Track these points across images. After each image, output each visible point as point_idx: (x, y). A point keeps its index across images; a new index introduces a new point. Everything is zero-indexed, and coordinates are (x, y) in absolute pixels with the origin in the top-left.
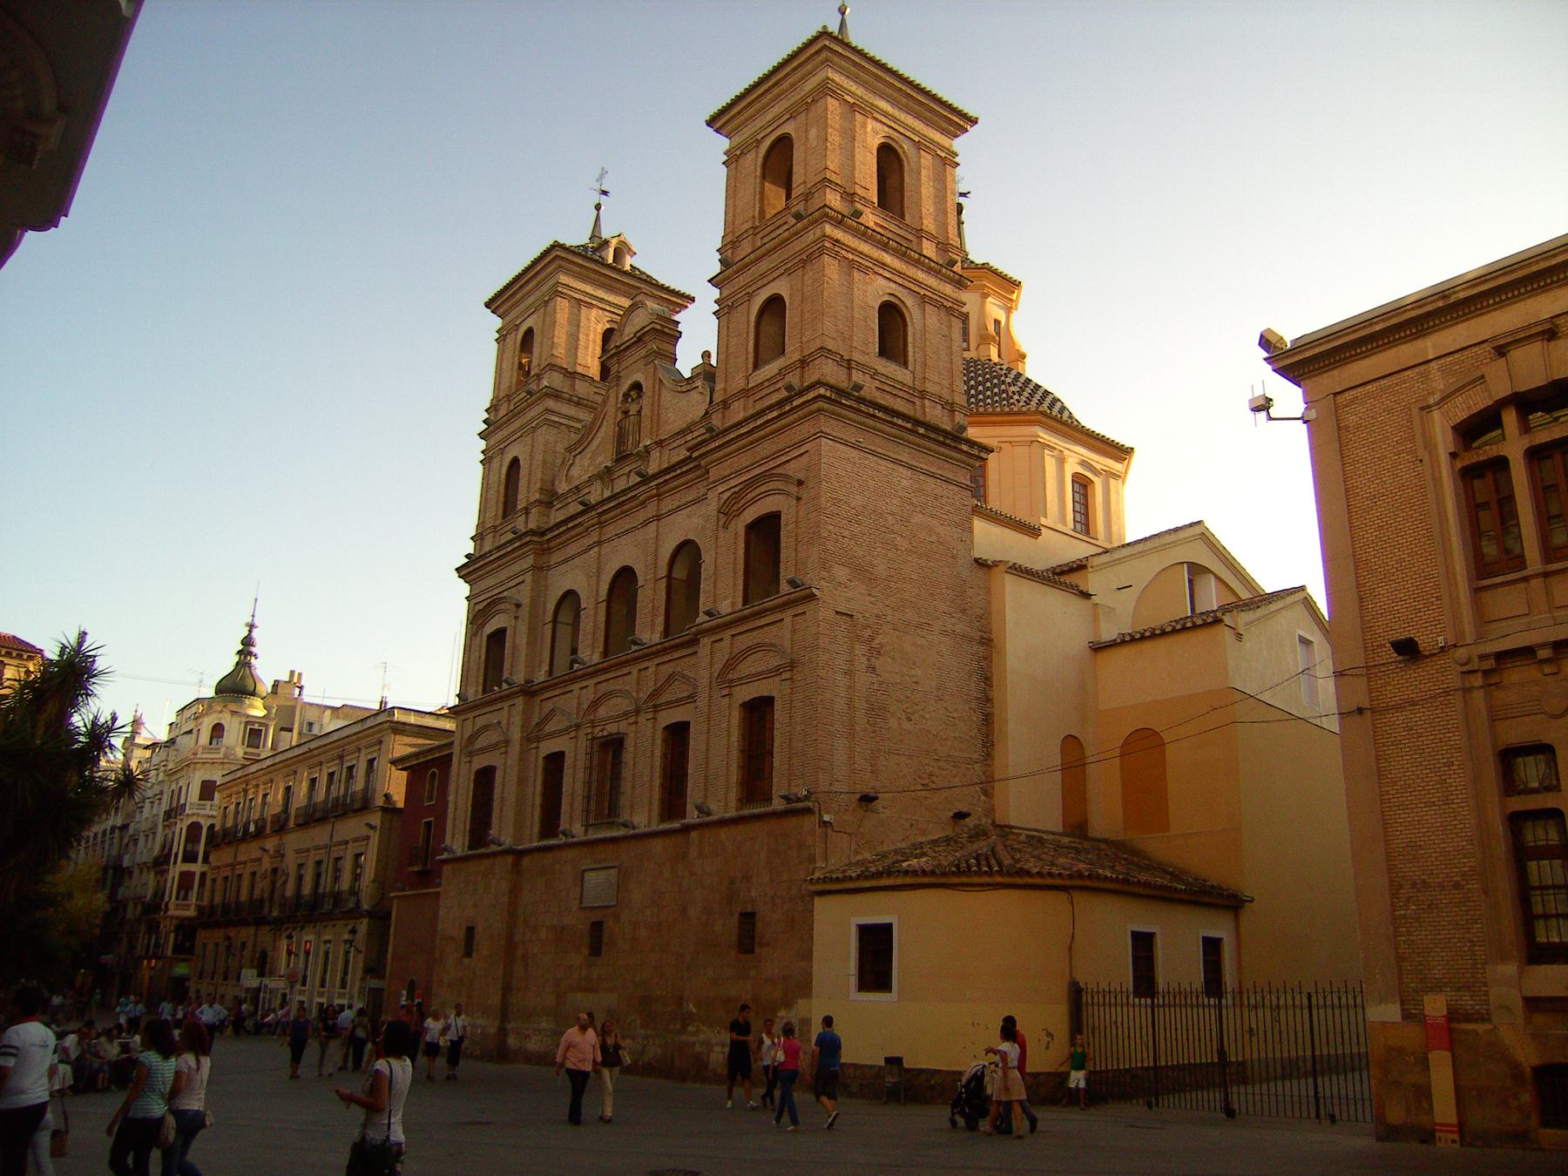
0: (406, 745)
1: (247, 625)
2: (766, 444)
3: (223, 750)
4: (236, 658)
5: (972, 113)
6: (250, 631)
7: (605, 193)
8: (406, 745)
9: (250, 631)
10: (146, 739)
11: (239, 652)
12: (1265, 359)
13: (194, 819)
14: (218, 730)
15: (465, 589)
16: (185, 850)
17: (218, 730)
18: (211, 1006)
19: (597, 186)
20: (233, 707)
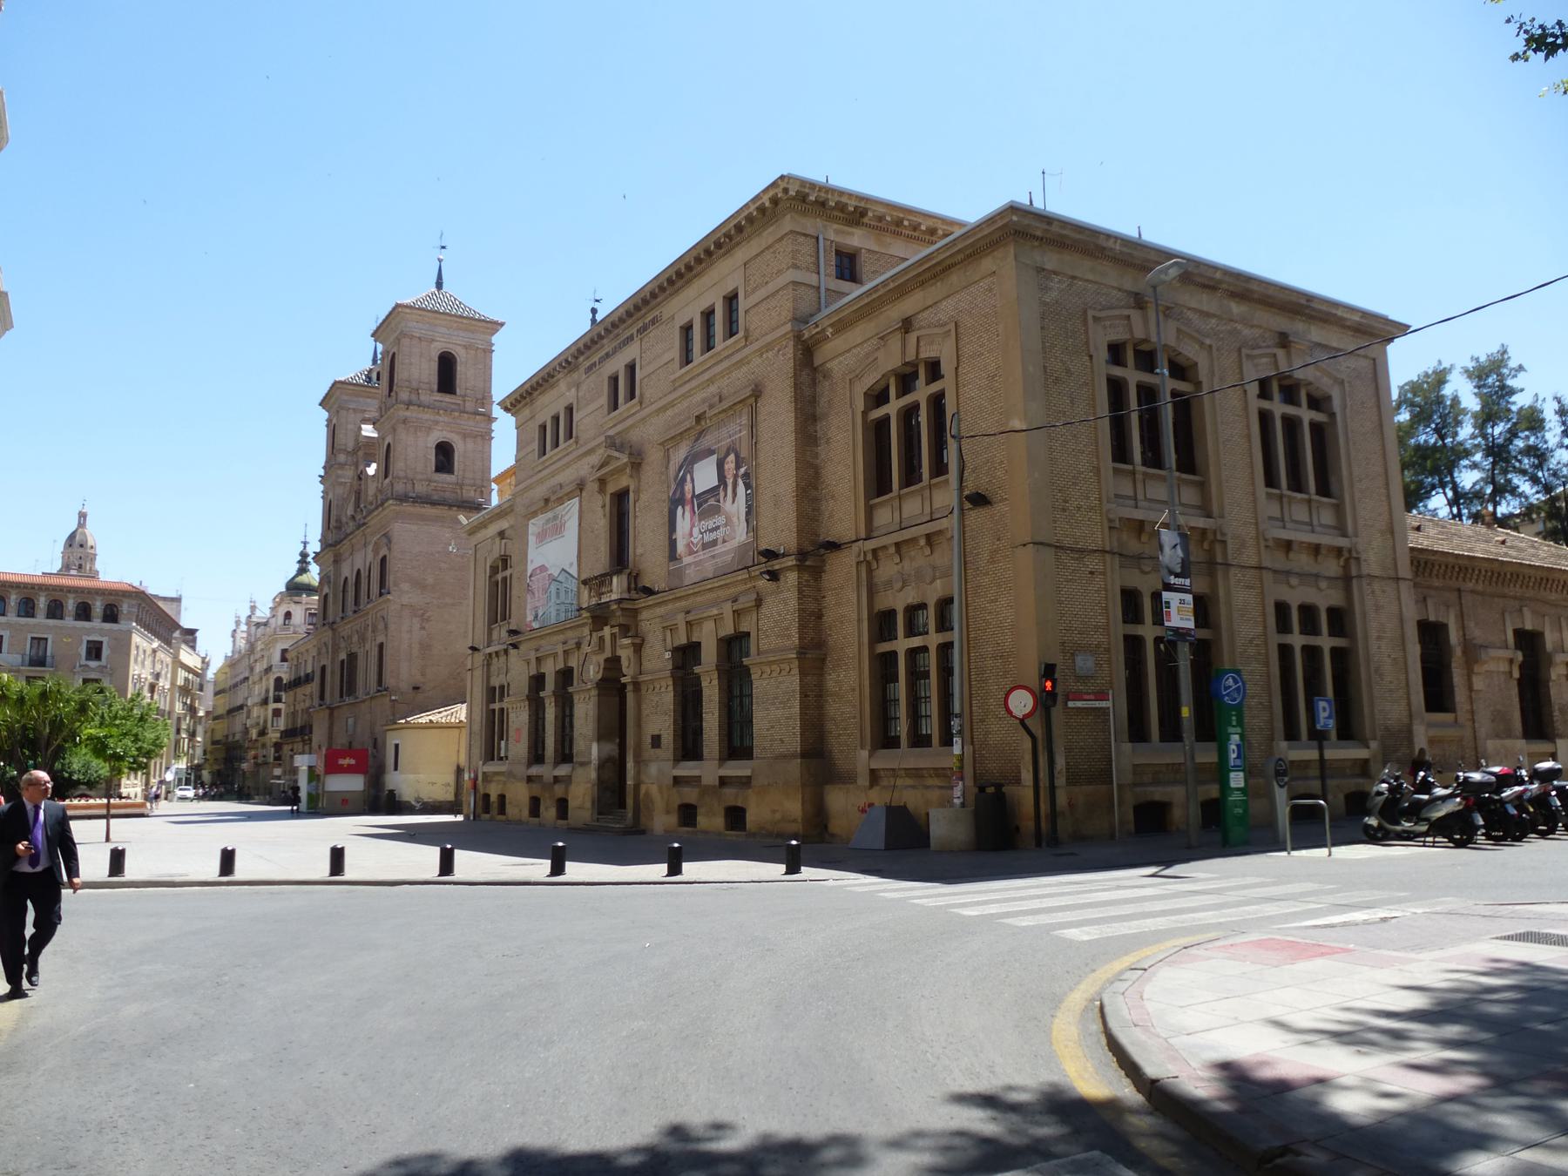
0: (1497, 938)
1: (302, 542)
2: (693, 381)
3: (292, 629)
4: (297, 566)
6: (305, 547)
7: (597, 301)
8: (1497, 938)
9: (305, 547)
10: (259, 617)
11: (299, 562)
12: (1547, 58)
13: (278, 675)
14: (288, 615)
15: (325, 415)
16: (274, 696)
17: (288, 615)
18: (1518, 487)
19: (592, 298)
20: (296, 599)
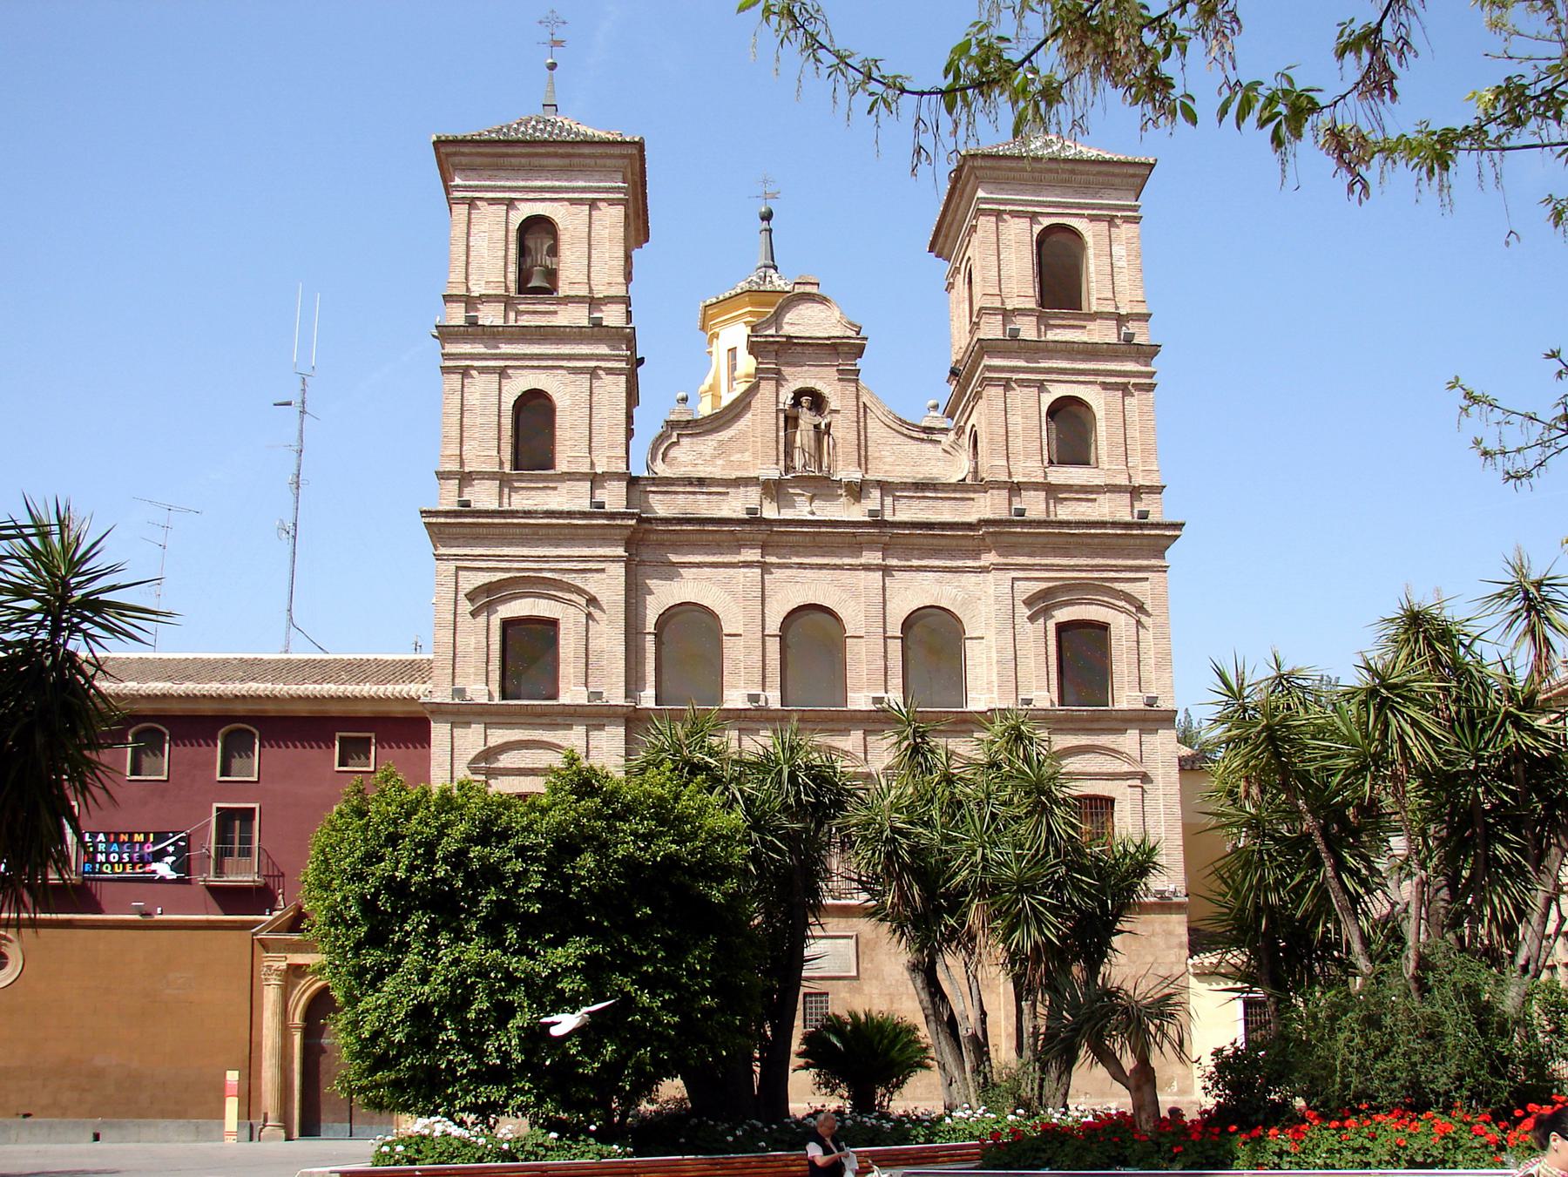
5: (1179, 521)
